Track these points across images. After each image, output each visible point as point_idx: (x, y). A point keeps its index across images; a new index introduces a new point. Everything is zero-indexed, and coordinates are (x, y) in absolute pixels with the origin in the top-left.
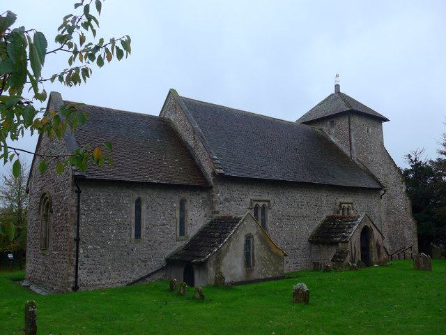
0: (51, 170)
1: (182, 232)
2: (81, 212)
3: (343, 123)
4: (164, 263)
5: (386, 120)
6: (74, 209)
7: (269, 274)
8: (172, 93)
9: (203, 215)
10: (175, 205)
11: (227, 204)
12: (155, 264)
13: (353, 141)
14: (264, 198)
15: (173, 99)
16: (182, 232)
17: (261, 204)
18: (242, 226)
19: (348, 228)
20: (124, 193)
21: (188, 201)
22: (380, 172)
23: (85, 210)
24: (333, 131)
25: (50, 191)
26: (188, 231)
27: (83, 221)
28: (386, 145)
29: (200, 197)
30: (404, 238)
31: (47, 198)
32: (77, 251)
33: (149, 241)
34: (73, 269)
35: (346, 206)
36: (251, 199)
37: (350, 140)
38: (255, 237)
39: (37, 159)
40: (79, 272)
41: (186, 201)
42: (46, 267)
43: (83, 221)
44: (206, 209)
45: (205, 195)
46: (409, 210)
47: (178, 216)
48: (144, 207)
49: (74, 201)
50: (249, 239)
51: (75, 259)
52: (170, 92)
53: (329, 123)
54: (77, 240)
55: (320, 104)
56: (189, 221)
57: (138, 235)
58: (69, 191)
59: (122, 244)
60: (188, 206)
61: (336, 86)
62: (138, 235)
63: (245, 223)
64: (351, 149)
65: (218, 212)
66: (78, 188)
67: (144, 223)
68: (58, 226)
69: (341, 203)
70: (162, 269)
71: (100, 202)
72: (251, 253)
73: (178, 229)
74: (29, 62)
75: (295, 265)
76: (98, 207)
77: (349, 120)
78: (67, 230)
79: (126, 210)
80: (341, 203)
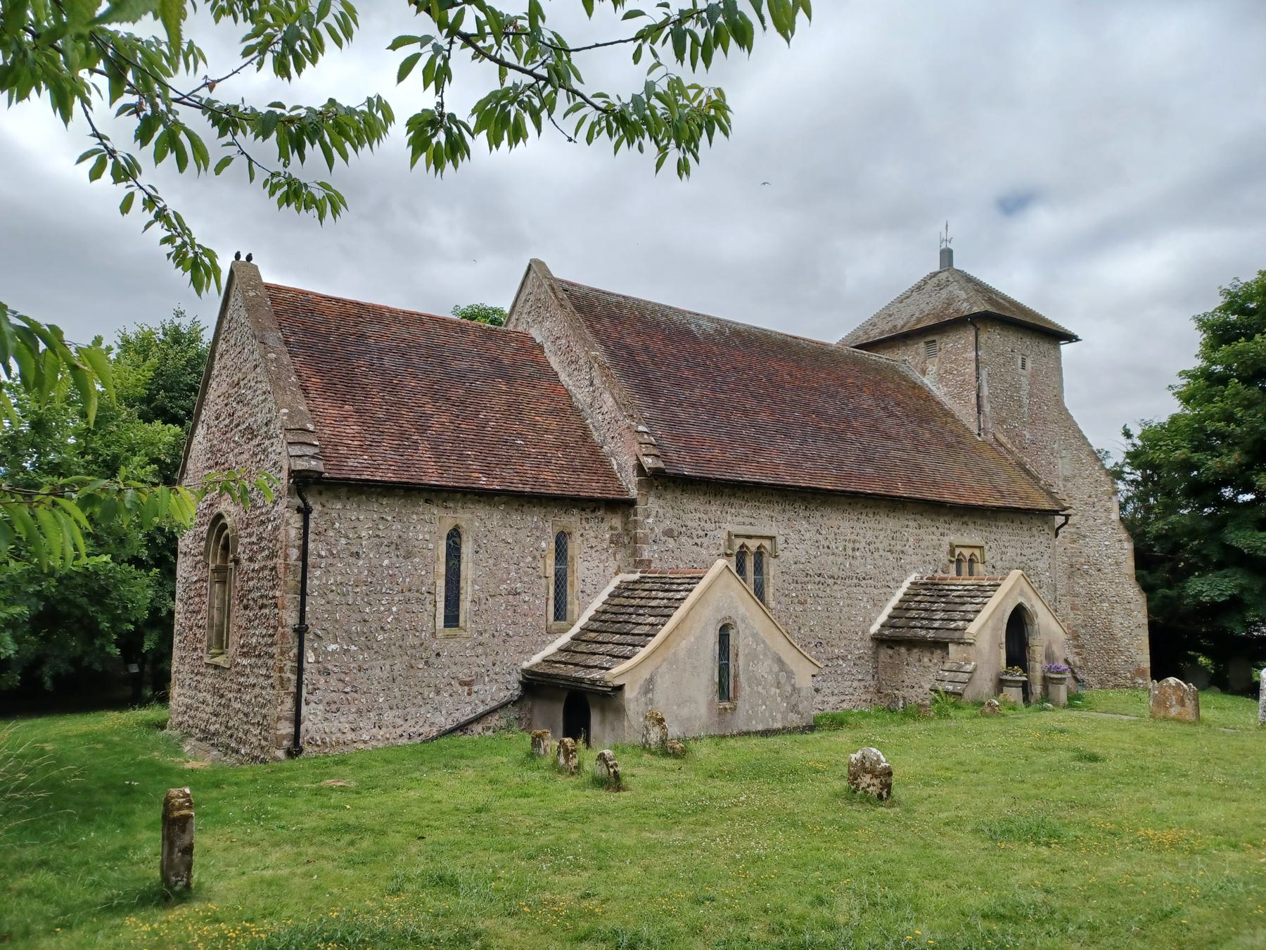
1: (560, 613)
3: (960, 345)
8: (535, 269)
11: (671, 543)
13: (985, 391)
16: (560, 613)
17: (753, 545)
21: (577, 535)
23: (320, 556)
27: (316, 582)
29: (605, 526)
32: (300, 657)
37: (979, 389)
40: (304, 709)
44: (618, 557)
45: (616, 521)
46: (1129, 565)
47: (551, 571)
48: (467, 549)
51: (294, 677)
54: (301, 631)
56: (578, 586)
57: (452, 619)
59: (411, 640)
60: (575, 547)
62: (452, 619)
73: (551, 603)
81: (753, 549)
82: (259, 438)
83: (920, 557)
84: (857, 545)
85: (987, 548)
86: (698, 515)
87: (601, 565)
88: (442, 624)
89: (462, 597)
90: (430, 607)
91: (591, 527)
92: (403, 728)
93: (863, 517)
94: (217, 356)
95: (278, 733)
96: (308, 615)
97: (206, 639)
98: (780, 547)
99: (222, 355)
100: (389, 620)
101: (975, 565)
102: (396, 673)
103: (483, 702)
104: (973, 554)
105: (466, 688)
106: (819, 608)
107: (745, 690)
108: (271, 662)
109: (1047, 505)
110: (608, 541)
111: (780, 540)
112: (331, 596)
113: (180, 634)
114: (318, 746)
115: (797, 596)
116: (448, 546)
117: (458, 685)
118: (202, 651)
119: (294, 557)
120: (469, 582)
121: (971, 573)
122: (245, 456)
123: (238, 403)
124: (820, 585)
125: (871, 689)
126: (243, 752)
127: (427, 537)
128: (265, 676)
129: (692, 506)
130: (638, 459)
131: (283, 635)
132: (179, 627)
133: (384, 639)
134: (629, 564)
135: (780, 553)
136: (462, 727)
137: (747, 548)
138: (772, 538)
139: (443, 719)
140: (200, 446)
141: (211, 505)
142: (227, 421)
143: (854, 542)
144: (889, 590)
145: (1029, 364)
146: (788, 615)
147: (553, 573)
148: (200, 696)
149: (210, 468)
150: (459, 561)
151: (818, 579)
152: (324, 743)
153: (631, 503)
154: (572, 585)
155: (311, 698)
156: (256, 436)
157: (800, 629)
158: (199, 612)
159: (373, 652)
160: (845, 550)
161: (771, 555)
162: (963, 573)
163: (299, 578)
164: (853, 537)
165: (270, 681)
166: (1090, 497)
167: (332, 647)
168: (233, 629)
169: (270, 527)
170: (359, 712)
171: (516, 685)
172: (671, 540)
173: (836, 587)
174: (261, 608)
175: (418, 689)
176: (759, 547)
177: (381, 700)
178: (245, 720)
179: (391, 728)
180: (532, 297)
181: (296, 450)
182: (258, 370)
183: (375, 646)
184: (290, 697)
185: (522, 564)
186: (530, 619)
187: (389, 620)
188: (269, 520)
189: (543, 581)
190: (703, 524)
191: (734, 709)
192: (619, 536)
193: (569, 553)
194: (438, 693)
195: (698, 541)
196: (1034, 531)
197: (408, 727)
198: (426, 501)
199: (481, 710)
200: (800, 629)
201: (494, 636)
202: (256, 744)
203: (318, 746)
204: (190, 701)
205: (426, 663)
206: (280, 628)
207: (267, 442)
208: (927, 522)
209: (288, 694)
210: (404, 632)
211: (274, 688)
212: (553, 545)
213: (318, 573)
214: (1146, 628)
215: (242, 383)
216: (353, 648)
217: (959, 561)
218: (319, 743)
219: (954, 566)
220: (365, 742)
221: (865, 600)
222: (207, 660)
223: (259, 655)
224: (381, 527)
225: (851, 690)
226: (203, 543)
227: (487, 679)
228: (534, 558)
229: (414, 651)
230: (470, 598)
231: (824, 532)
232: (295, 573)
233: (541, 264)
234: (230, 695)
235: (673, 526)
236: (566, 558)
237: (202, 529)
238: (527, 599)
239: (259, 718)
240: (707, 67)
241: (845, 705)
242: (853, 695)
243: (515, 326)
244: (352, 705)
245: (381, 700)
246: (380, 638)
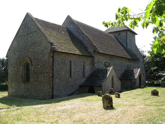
5: (136, 34)
8: (28, 16)
13: (128, 42)
15: (69, 19)
38: (114, 76)
45: (90, 60)
47: (82, 68)
51: (54, 85)
54: (53, 77)
69: (128, 65)
70: (77, 90)
80: (128, 65)
163: (52, 68)
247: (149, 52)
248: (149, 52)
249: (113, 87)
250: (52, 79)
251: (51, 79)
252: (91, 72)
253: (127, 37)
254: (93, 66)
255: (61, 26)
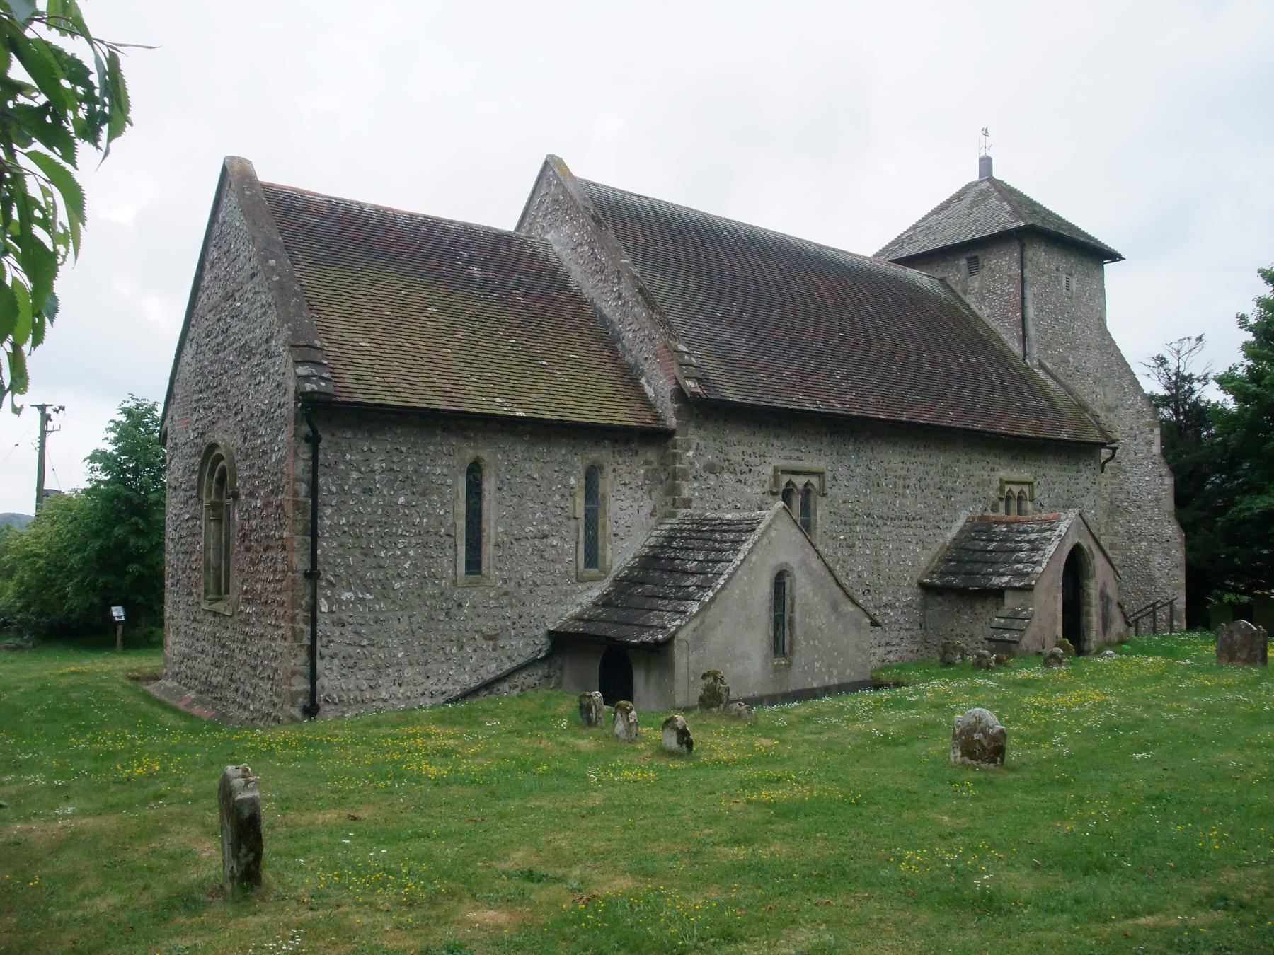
0: (231, 378)
1: (592, 557)
2: (322, 495)
3: (1003, 263)
4: (542, 645)
5: (1114, 257)
6: (303, 488)
7: (830, 677)
8: (552, 171)
9: (647, 509)
10: (572, 481)
11: (712, 481)
12: (522, 647)
13: (1031, 313)
14: (807, 464)
16: (592, 557)
17: (800, 481)
18: (765, 541)
19: (1032, 550)
20: (434, 445)
21: (608, 469)
22: (1096, 396)
23: (330, 492)
24: (975, 283)
25: (227, 438)
26: (609, 554)
27: (327, 522)
28: (1110, 327)
29: (639, 460)
30: (1151, 580)
31: (220, 458)
32: (313, 608)
33: (505, 581)
34: (303, 656)
35: (1016, 489)
36: (776, 469)
37: (1023, 308)
39: (189, 350)
40: (320, 665)
41: (601, 468)
42: (224, 646)
43: (327, 522)
44: (654, 495)
45: (652, 455)
46: (1169, 503)
47: (580, 512)
48: (489, 486)
49: (300, 466)
50: (780, 581)
51: (307, 629)
52: (546, 164)
53: (963, 262)
54: (312, 575)
55: (937, 211)
56: (610, 527)
57: (474, 565)
58: (285, 437)
59: (430, 589)
60: (607, 484)
61: (981, 160)
62: (474, 565)
63: (773, 534)
64: (1024, 336)
65: (687, 503)
66: (314, 431)
67: (492, 530)
68: (254, 536)
69: (1004, 483)
71: (372, 471)
72: (787, 618)
73: (581, 547)
74: (71, 240)
75: (882, 650)
76: (366, 485)
77: (1022, 253)
78: (284, 548)
79: (442, 495)
81: (800, 486)
82: (258, 356)
83: (970, 495)
84: (907, 482)
85: (1035, 484)
86: (742, 448)
87: (635, 505)
88: (464, 571)
89: (484, 540)
90: (450, 552)
91: (625, 462)
92: (424, 686)
93: (914, 451)
94: (208, 265)
95: (294, 689)
96: (320, 559)
97: (202, 582)
98: (828, 484)
99: (212, 266)
100: (406, 566)
101: (1023, 503)
102: (415, 626)
103: (509, 658)
104: (1022, 491)
105: (491, 643)
106: (868, 552)
107: (802, 643)
108: (280, 611)
109: (1103, 440)
110: (642, 478)
111: (829, 476)
112: (343, 539)
113: (173, 577)
114: (336, 704)
115: (845, 539)
116: (469, 484)
117: (481, 639)
118: (199, 596)
119: (303, 493)
120: (492, 524)
121: (1020, 512)
122: (240, 379)
123: (233, 317)
124: (869, 527)
125: (918, 639)
126: (251, 708)
127: (446, 471)
128: (275, 626)
129: (734, 438)
130: (677, 383)
131: (294, 581)
132: (171, 570)
133: (401, 587)
134: (666, 503)
135: (828, 490)
136: (488, 686)
137: (794, 485)
138: (819, 474)
139: (467, 676)
140: (188, 368)
141: (203, 434)
142: (220, 339)
143: (904, 479)
144: (938, 531)
145: (1074, 285)
146: (836, 559)
147: (583, 514)
148: (199, 645)
149: (201, 392)
150: (480, 499)
151: (866, 520)
152: (341, 701)
153: (668, 434)
154: (604, 527)
155: (324, 651)
156: (254, 355)
157: (847, 575)
158: (192, 553)
159: (390, 601)
160: (895, 487)
161: (818, 493)
162: (1012, 512)
163: (309, 517)
164: (903, 473)
165: (281, 632)
166: (1132, 429)
167: (346, 596)
168: (234, 573)
169: (274, 459)
170: (377, 668)
171: (544, 640)
172: (712, 476)
173: (885, 529)
174: (265, 550)
175: (439, 643)
176: (806, 485)
177: (400, 655)
178: (252, 672)
179: (411, 686)
180: (549, 199)
181: (302, 370)
182: (256, 279)
183: (392, 595)
184: (303, 650)
185: (549, 504)
186: (558, 566)
187: (406, 566)
188: (273, 451)
189: (573, 523)
190: (747, 458)
191: (790, 665)
192: (655, 470)
193: (601, 491)
194: (461, 648)
195: (742, 477)
196: (1082, 467)
197: (430, 685)
198: (444, 430)
199: (507, 666)
200: (847, 575)
201: (519, 585)
202: (267, 699)
203: (336, 704)
204: (187, 650)
205: (447, 614)
206: (290, 573)
207: (268, 362)
208: (976, 456)
209: (302, 646)
210: (422, 580)
211: (285, 639)
212: (583, 482)
213: (329, 511)
214: (1184, 568)
215: (237, 295)
216: (368, 596)
217: (1008, 498)
218: (337, 701)
219: (1004, 503)
220: (385, 701)
221: (914, 542)
222: (204, 606)
223: (266, 602)
224: (395, 459)
225: (898, 640)
226: (195, 477)
227: (513, 632)
228: (562, 496)
229: (434, 602)
230: (493, 542)
231: (873, 468)
232: (305, 510)
233: (559, 162)
234: (234, 646)
235: (715, 461)
236: (597, 496)
237: (193, 460)
238: (555, 543)
239: (269, 672)
240: (52, 324)
241: (891, 657)
242: (899, 645)
243: (529, 231)
244: (370, 661)
245: (400, 655)
246: (397, 586)
247: (1225, 381)
248: (1225, 381)
249: (293, 627)
250: (309, 590)
251: (304, 589)
252: (652, 541)
253: (1023, 281)
254: (669, 499)
255: (500, 238)
